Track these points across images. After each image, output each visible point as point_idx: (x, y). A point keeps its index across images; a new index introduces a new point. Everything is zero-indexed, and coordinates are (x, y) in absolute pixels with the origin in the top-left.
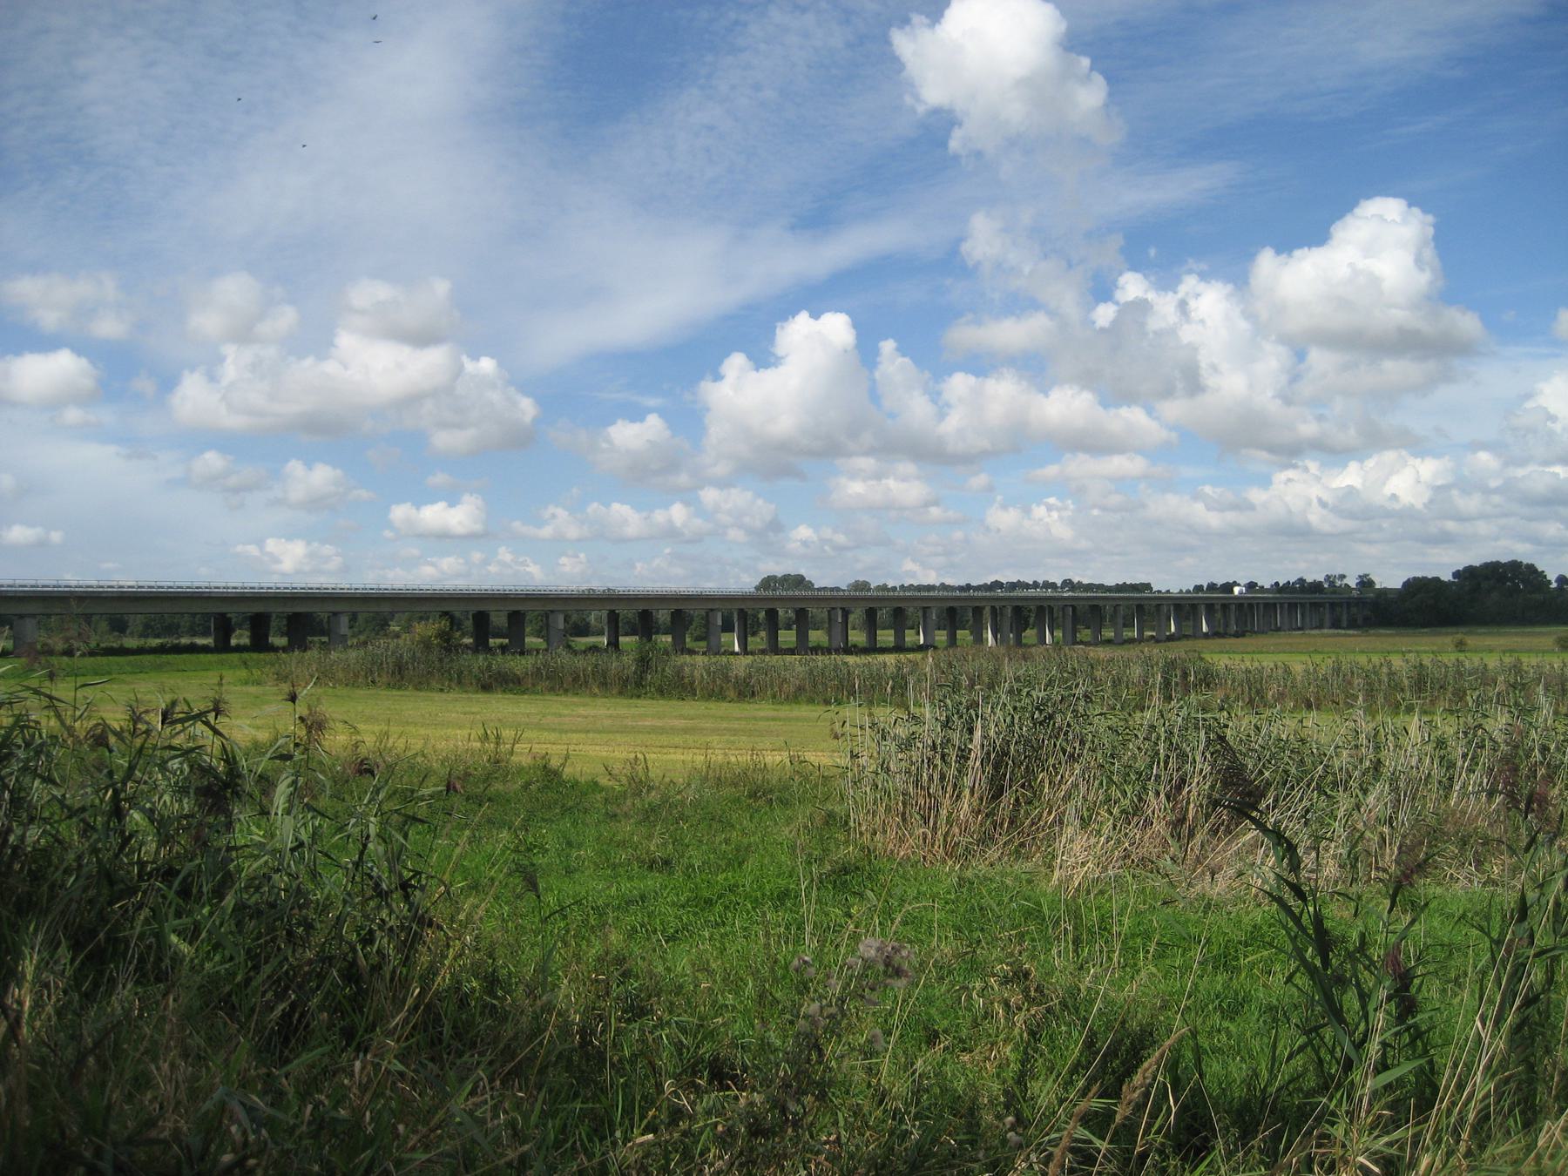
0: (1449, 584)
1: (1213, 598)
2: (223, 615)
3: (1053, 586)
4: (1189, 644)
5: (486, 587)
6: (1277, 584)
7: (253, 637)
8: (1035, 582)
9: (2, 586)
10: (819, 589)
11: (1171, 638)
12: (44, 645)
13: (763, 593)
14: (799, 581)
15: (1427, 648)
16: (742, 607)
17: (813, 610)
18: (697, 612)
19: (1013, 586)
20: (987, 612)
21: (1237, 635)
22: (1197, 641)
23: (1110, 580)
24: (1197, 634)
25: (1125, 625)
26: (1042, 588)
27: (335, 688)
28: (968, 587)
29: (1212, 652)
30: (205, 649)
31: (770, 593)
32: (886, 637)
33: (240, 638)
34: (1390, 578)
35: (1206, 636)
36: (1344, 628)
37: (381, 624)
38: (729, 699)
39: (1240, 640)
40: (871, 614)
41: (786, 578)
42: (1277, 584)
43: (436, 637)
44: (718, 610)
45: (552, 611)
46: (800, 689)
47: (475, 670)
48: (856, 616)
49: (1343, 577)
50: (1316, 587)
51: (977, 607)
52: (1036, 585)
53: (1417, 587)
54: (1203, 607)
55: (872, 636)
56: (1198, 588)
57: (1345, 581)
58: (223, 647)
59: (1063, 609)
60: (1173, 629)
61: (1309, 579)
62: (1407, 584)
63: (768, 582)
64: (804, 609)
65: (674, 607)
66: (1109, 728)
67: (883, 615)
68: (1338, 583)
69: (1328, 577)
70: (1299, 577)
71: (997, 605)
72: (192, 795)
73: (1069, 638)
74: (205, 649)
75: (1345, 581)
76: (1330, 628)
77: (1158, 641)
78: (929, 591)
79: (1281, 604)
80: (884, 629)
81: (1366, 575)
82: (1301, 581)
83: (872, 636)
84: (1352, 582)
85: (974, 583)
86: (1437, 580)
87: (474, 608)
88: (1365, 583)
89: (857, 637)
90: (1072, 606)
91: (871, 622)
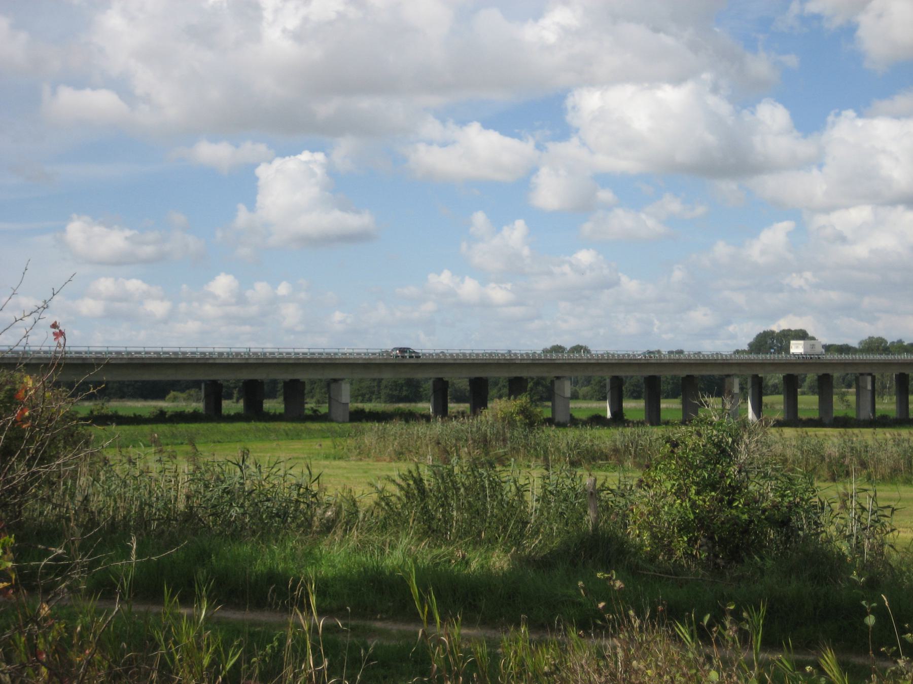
2: (214, 382)
7: (247, 406)
9: (3, 352)
13: (753, 357)
18: (461, 381)
30: (194, 417)
31: (761, 357)
38: (822, 478)
45: (558, 378)
46: (895, 471)
47: (563, 446)
51: (295, 382)
58: (214, 414)
64: (297, 381)
72: (481, 615)
74: (194, 417)
76: (385, 402)
78: (847, 353)
80: (667, 397)
87: (433, 374)
90: (870, 374)
91: (824, 386)
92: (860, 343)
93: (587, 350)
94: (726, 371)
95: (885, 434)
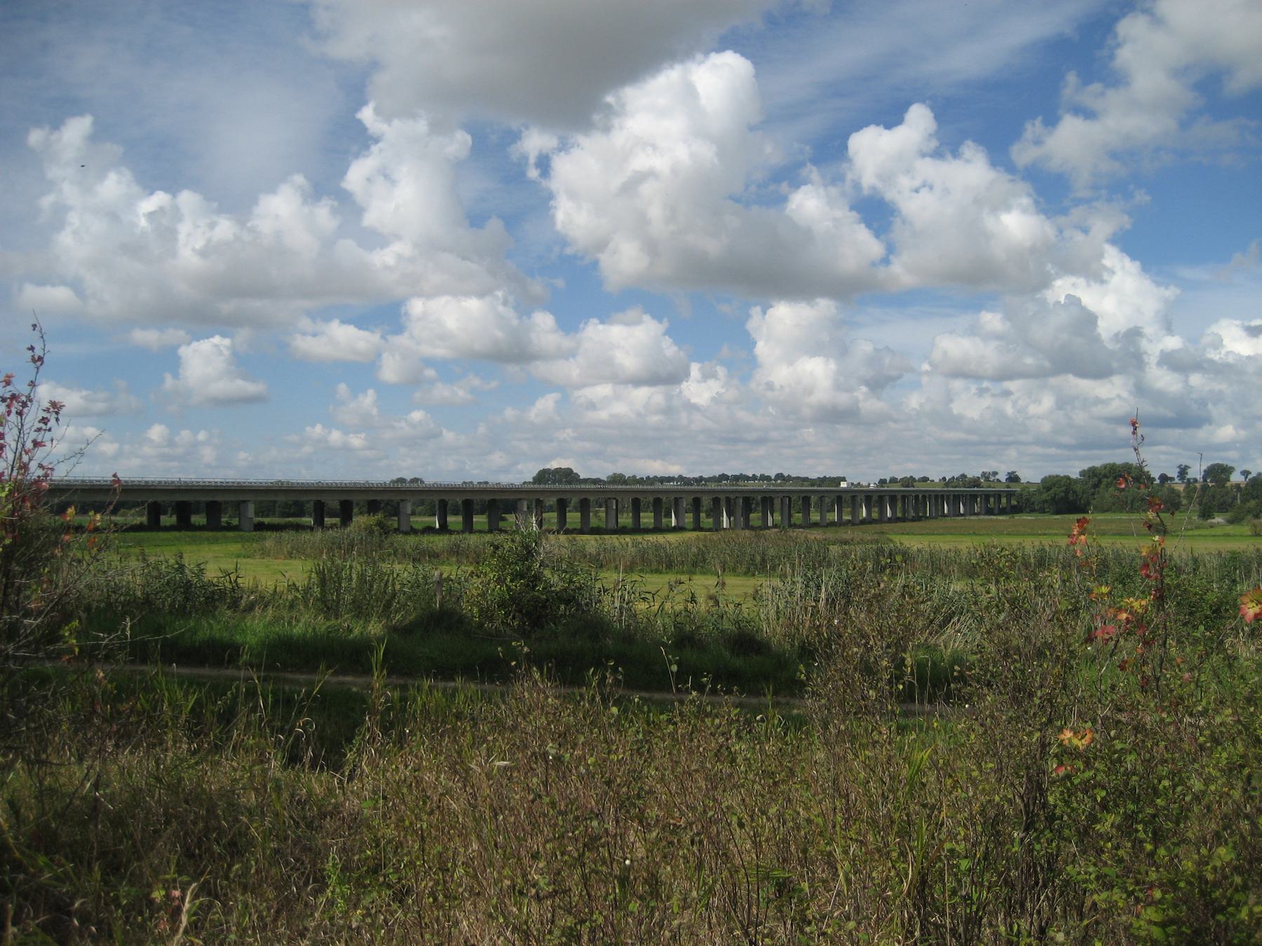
0: (1076, 481)
1: (909, 491)
3: (768, 478)
4: (877, 527)
5: (251, 481)
6: (944, 479)
7: (179, 519)
8: (754, 475)
10: (586, 481)
11: (863, 522)
12: (1068, 296)
14: (568, 475)
15: (1057, 532)
16: (319, 499)
17: (844, 496)
19: (737, 478)
20: (723, 503)
21: (913, 520)
22: (883, 525)
23: (814, 475)
24: (882, 520)
25: (829, 511)
26: (759, 480)
27: (714, 692)
28: (724, 477)
29: (896, 534)
32: (647, 519)
33: (167, 520)
34: (1031, 475)
35: (890, 520)
36: (994, 515)
37: (346, 512)
39: (915, 524)
40: (697, 503)
41: (558, 471)
42: (944, 479)
43: (375, 525)
44: (525, 499)
48: (627, 502)
49: (995, 473)
50: (975, 482)
52: (754, 478)
53: (1050, 483)
54: (888, 498)
55: (637, 518)
56: (883, 482)
57: (997, 477)
59: (606, 501)
60: (864, 515)
61: (970, 476)
62: (1044, 480)
63: (543, 476)
65: (583, 497)
66: (1013, 602)
67: (706, 502)
68: (992, 478)
69: (984, 474)
70: (961, 473)
71: (732, 496)
73: (786, 522)
75: (997, 477)
77: (853, 524)
79: (904, 497)
81: (1013, 473)
82: (963, 476)
83: (637, 518)
84: (1003, 477)
85: (705, 476)
86: (1068, 478)
87: (314, 498)
88: (1013, 478)
89: (626, 519)
91: (637, 507)
92: (608, 478)
93: (422, 482)
94: (403, 497)
95: (628, 539)
